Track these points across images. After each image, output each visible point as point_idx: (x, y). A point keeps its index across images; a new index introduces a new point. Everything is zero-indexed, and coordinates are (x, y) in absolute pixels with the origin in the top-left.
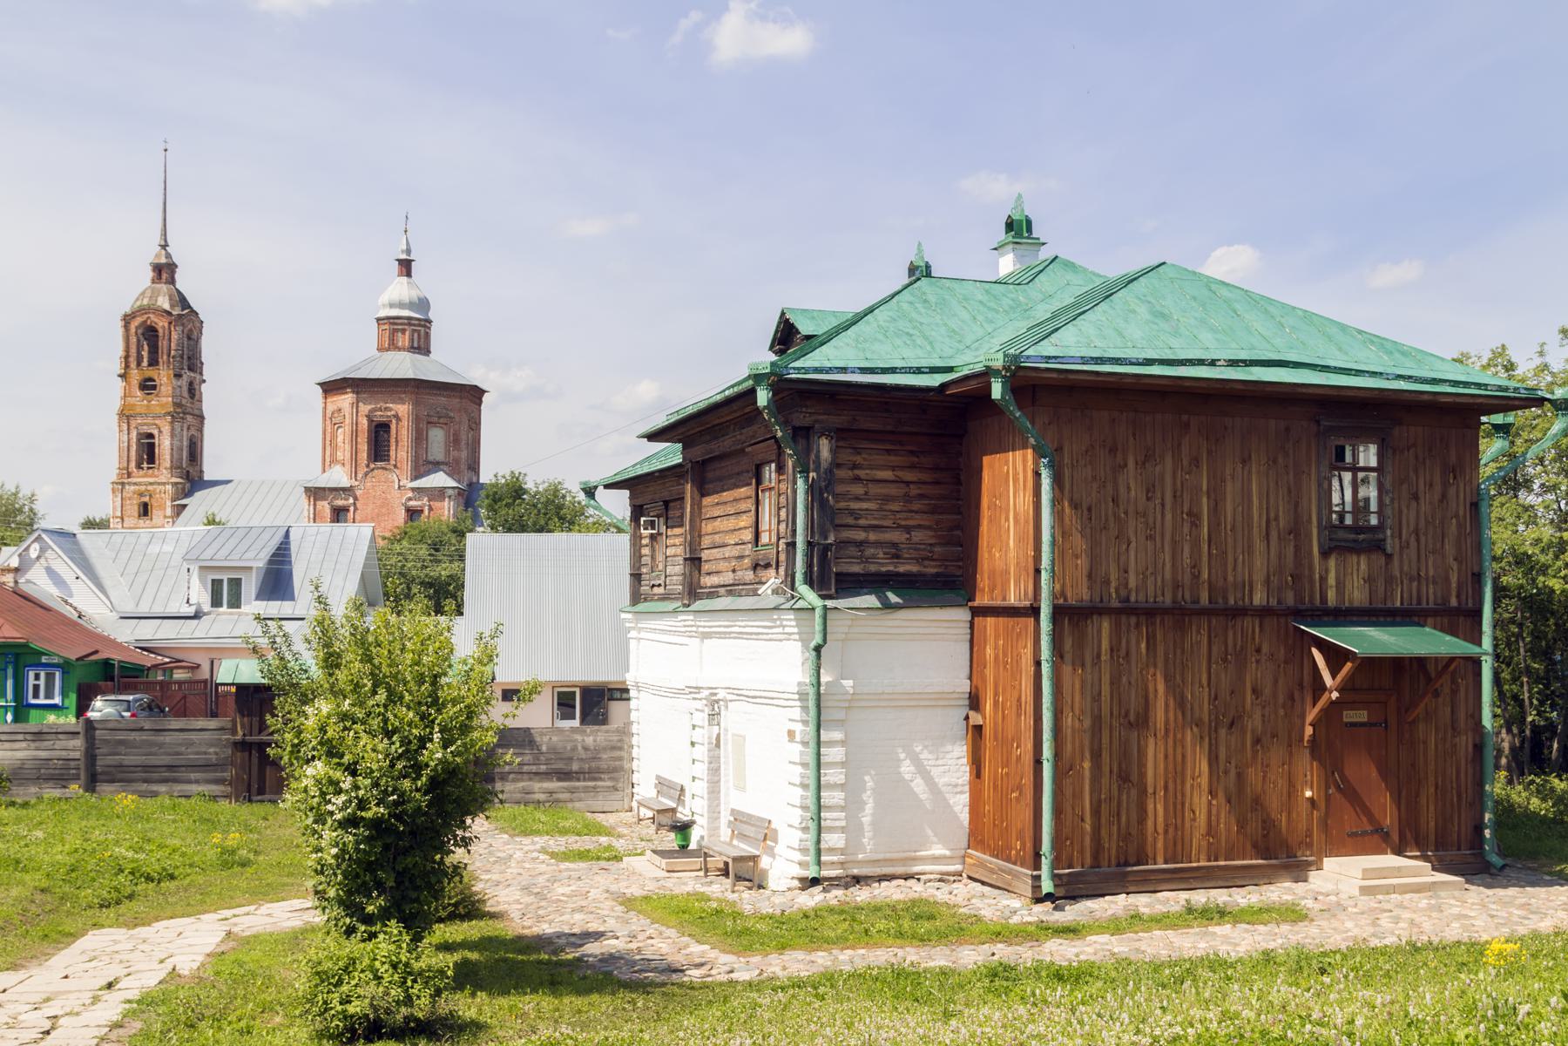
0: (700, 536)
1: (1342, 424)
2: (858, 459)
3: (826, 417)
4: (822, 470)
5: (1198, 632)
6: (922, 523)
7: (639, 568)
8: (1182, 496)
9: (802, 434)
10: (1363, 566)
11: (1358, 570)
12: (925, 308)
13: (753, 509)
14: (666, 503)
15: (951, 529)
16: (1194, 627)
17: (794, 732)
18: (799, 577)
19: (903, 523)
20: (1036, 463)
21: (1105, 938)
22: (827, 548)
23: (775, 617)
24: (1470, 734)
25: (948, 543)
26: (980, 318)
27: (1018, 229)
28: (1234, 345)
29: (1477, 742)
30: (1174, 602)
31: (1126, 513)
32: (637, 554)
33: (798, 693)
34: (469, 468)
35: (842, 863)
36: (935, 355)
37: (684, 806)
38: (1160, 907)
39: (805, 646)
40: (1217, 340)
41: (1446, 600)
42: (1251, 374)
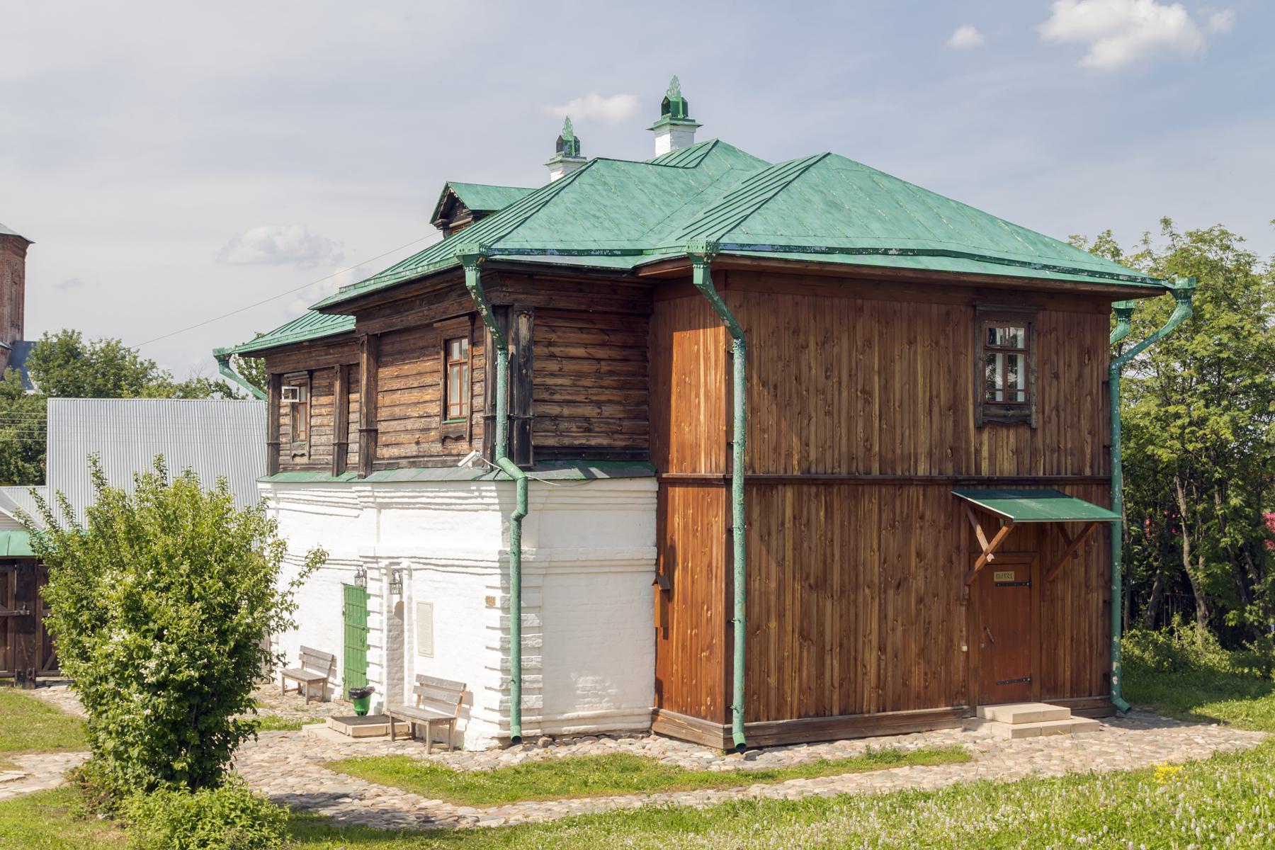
0: (376, 408)
1: (994, 309)
2: (554, 337)
3: (525, 296)
4: (521, 347)
5: (870, 501)
6: (611, 398)
7: (278, 438)
8: (856, 375)
9: (502, 312)
10: (1012, 440)
11: (1007, 443)
12: (605, 190)
13: (442, 383)
14: (311, 373)
15: (638, 404)
16: (866, 496)
17: (494, 598)
18: (499, 449)
19: (594, 398)
20: (728, 344)
21: (801, 782)
22: (525, 423)
23: (473, 488)
24: (1100, 591)
25: (635, 418)
26: (657, 201)
27: (673, 110)
28: (901, 235)
29: (1106, 598)
30: (849, 474)
31: (808, 391)
32: (276, 424)
33: (498, 561)
34: (12, 325)
35: (539, 723)
36: (623, 238)
37: (335, 677)
38: (840, 754)
39: (505, 518)
40: (887, 230)
41: (1081, 471)
42: (920, 263)
